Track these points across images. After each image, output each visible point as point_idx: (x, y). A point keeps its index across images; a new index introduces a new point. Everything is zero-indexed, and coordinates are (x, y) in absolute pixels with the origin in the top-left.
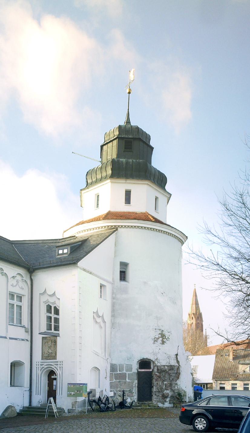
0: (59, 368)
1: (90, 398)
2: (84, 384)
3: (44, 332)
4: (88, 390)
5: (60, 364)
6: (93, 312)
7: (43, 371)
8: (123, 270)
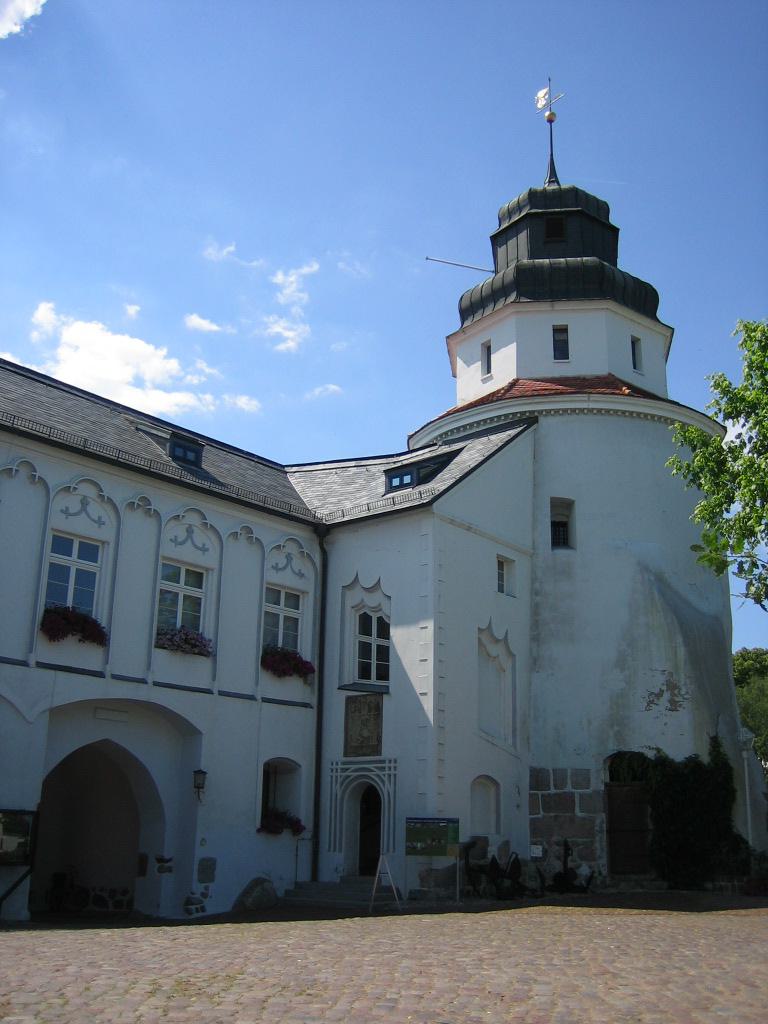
0: (386, 779)
1: (471, 861)
2: (450, 821)
3: (351, 682)
4: (464, 838)
5: (390, 768)
6: (479, 629)
7: (347, 787)
8: (559, 519)
